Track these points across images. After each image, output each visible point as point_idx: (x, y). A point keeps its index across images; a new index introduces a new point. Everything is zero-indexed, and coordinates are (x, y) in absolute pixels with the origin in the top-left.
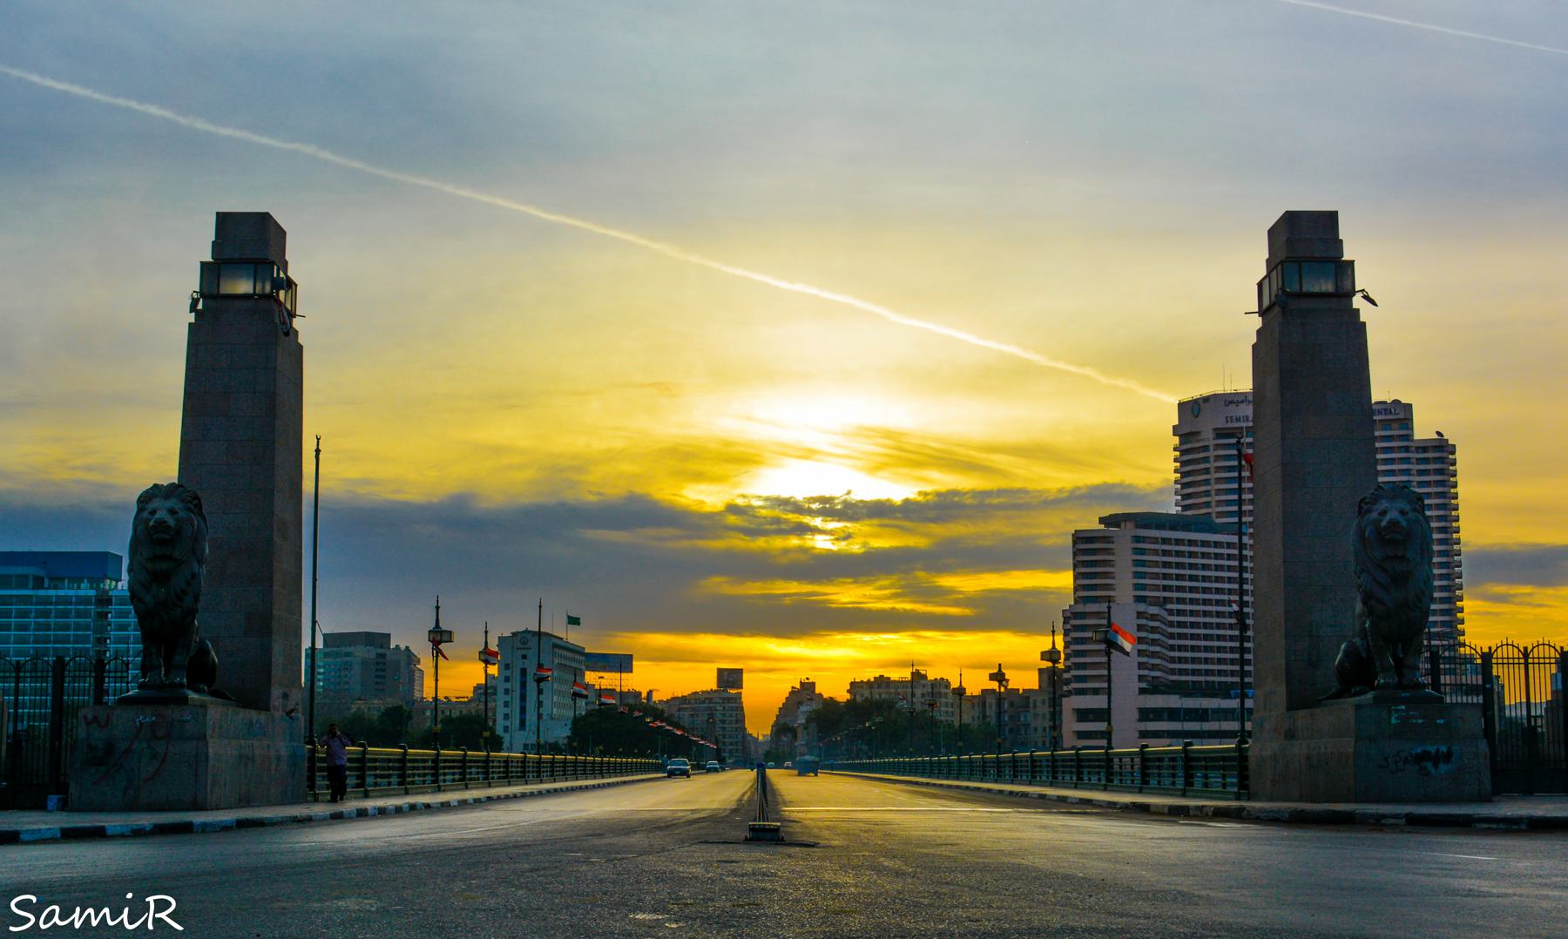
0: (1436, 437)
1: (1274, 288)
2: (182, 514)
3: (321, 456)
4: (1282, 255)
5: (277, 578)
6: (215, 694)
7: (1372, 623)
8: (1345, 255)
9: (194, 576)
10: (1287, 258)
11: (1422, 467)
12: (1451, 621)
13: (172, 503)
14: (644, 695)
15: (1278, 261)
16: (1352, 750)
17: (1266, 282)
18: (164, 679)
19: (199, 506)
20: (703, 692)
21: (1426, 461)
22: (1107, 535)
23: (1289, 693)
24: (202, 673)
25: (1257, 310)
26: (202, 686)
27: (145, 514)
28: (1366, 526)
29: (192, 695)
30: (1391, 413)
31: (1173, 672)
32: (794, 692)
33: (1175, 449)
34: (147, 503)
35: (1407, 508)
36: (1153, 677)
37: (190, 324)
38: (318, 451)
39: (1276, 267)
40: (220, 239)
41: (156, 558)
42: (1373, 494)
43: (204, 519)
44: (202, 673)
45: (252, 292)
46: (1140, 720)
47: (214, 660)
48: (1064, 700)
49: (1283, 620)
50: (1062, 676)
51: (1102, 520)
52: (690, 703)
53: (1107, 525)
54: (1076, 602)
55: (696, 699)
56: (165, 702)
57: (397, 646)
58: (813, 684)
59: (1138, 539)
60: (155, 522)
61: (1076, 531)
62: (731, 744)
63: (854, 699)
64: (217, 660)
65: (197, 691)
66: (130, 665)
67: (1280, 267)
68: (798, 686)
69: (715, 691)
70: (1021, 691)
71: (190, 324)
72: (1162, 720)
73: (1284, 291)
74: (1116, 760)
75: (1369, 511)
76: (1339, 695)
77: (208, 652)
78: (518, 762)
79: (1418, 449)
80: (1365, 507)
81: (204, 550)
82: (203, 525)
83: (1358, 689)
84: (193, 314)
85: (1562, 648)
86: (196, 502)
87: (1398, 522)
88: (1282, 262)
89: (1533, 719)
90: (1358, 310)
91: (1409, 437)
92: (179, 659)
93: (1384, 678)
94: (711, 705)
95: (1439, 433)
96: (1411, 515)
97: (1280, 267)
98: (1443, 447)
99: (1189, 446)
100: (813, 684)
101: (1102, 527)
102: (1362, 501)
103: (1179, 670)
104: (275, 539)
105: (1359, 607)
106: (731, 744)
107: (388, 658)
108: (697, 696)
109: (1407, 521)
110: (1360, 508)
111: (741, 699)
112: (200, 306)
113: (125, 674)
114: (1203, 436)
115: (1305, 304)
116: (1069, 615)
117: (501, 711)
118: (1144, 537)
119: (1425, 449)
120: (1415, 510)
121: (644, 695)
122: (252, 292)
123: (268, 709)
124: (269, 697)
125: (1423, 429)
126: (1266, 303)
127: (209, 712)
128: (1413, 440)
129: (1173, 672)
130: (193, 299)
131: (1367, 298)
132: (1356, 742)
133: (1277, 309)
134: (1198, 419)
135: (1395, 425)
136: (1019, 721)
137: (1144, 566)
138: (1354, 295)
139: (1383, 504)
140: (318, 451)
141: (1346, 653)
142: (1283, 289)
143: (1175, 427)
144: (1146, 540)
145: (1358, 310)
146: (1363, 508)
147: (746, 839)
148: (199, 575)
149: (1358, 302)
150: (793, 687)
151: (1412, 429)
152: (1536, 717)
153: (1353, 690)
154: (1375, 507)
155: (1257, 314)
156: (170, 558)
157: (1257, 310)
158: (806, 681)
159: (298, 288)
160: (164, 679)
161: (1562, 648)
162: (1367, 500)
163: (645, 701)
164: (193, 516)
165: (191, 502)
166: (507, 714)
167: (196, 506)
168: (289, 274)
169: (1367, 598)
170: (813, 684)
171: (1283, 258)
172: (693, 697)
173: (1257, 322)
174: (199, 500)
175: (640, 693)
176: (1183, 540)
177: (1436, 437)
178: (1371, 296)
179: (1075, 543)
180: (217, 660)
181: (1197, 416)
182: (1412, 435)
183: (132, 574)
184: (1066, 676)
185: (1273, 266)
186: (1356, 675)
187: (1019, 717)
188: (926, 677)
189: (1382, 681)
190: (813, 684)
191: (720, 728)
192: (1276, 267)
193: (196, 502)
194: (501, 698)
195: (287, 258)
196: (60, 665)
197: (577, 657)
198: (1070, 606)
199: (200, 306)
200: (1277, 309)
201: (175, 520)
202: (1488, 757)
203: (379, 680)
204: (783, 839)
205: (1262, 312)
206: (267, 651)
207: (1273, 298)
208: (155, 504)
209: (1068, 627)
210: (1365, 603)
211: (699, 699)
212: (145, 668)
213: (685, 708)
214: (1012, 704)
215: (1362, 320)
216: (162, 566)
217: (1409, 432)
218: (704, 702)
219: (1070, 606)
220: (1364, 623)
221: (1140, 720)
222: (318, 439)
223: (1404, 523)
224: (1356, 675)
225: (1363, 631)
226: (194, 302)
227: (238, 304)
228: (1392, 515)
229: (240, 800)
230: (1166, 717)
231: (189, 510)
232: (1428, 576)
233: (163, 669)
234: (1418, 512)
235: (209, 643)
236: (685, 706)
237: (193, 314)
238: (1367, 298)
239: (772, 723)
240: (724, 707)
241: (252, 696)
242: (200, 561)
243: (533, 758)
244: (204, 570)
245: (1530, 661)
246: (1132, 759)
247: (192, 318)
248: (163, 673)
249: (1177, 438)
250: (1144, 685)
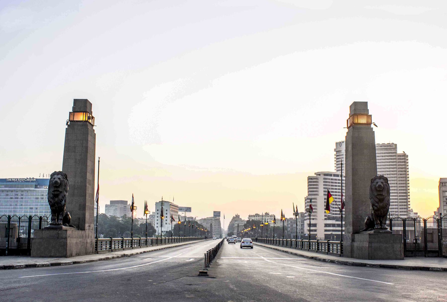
0: (403, 153)
1: (351, 122)
2: (62, 179)
3: (100, 162)
4: (353, 113)
5: (87, 195)
6: (70, 226)
7: (374, 211)
8: (369, 113)
9: (64, 196)
10: (354, 114)
11: (399, 161)
12: (407, 202)
13: (59, 176)
14: (194, 218)
15: (352, 114)
16: (367, 246)
17: (349, 120)
18: (57, 222)
19: (66, 177)
20: (210, 217)
21: (401, 159)
22: (317, 177)
23: (353, 229)
24: (66, 221)
25: (347, 127)
26: (66, 224)
27: (52, 179)
28: (373, 186)
29: (64, 227)
30: (391, 146)
31: (334, 214)
32: (234, 218)
33: (335, 155)
34: (53, 176)
35: (383, 181)
36: (328, 215)
37: (66, 128)
38: (99, 161)
39: (351, 116)
40: (75, 106)
41: (54, 191)
42: (375, 178)
43: (68, 180)
44: (66, 221)
45: (82, 120)
46: (325, 227)
47: (70, 218)
48: (305, 221)
49: (352, 210)
50: (304, 214)
51: (315, 174)
52: (206, 220)
53: (317, 175)
54: (308, 195)
55: (208, 219)
56: (56, 229)
57: (129, 204)
58: (239, 216)
59: (325, 179)
60: (55, 181)
61: (308, 176)
62: (217, 231)
63: (249, 220)
64: (71, 218)
65: (65, 225)
66: (48, 218)
67: (352, 116)
68: (235, 216)
69: (213, 217)
70: (294, 219)
71: (66, 128)
72: (331, 227)
73: (353, 123)
74: (311, 243)
75: (373, 182)
76: (366, 230)
77: (68, 215)
78: (155, 240)
79: (399, 156)
80: (372, 181)
81: (67, 188)
82: (67, 182)
83: (370, 229)
84: (67, 126)
85: (424, 218)
86: (66, 176)
87: (381, 185)
88: (353, 115)
89: (416, 237)
90: (373, 128)
91: (396, 153)
92: (60, 217)
93: (377, 226)
94: (212, 221)
95: (404, 152)
96: (384, 183)
97: (352, 116)
98: (405, 155)
99: (338, 154)
100: (239, 216)
101: (315, 175)
102: (372, 180)
103: (335, 213)
104: (87, 185)
105: (371, 208)
106: (217, 231)
107: (127, 207)
108: (208, 218)
109: (383, 185)
110: (371, 181)
111: (220, 219)
112: (69, 124)
113: (47, 220)
114: (342, 152)
115: (359, 126)
116: (306, 199)
117: (156, 222)
118: (326, 178)
119: (400, 156)
120: (385, 182)
121: (194, 218)
122: (82, 120)
123: (84, 230)
124: (85, 227)
125: (400, 151)
126: (349, 125)
127: (68, 232)
128: (397, 154)
129: (334, 214)
130: (67, 122)
131: (375, 125)
132: (369, 244)
133: (352, 127)
134: (341, 147)
135: (392, 150)
136: (293, 226)
137: (326, 186)
138: (371, 124)
139: (377, 180)
140: (99, 161)
141: (368, 220)
142: (353, 122)
143: (335, 149)
144: (327, 179)
145: (373, 128)
146: (373, 181)
147: (198, 275)
148: (66, 195)
149: (372, 126)
150: (234, 216)
151: (397, 151)
152: (417, 237)
153: (369, 229)
154: (375, 181)
155: (347, 128)
156: (58, 191)
157: (347, 127)
158: (237, 215)
159: (95, 118)
160: (57, 222)
161: (424, 218)
162: (373, 179)
163: (194, 220)
164: (64, 179)
165: (64, 176)
166: (158, 223)
167: (65, 177)
168: (92, 115)
169: (373, 205)
170: (239, 216)
171: (353, 114)
172: (207, 219)
173: (347, 130)
174: (66, 175)
175: (193, 217)
176: (337, 179)
177: (403, 153)
178: (376, 124)
179: (308, 180)
180: (71, 218)
181: (341, 146)
182: (397, 152)
183: (49, 195)
184: (305, 215)
185: (351, 116)
186: (370, 225)
187: (293, 225)
188: (269, 214)
189: (376, 227)
190: (239, 216)
191: (214, 227)
192: (351, 116)
193: (66, 176)
194: (156, 218)
195: (92, 111)
196: (30, 218)
197: (176, 208)
198: (307, 196)
199: (69, 124)
200: (352, 127)
201: (60, 181)
202: (403, 248)
203: (124, 211)
204: (208, 275)
205: (348, 128)
206: (84, 215)
207: (350, 124)
208: (56, 176)
209: (306, 202)
210: (372, 206)
211: (209, 219)
212: (52, 220)
213: (205, 222)
214: (291, 222)
215: (373, 131)
216: (56, 193)
217: (396, 152)
218: (210, 220)
219: (307, 196)
220: (372, 212)
221: (325, 227)
222: (99, 158)
223: (382, 186)
224: (370, 225)
225: (372, 214)
226: (68, 122)
227: (78, 123)
228: (380, 183)
229: (76, 254)
230: (331, 226)
231: (64, 178)
232: (389, 199)
233: (56, 220)
234: (386, 183)
235: (68, 213)
236: (205, 221)
237: (67, 126)
238: (375, 125)
239: (228, 226)
240: (215, 222)
241: (80, 226)
242: (66, 192)
243: (160, 239)
244: (67, 194)
245: (416, 222)
246: (315, 243)
247: (67, 126)
248: (56, 221)
249: (335, 152)
250: (326, 218)
